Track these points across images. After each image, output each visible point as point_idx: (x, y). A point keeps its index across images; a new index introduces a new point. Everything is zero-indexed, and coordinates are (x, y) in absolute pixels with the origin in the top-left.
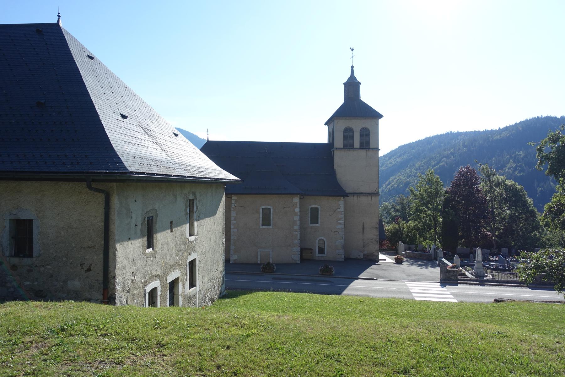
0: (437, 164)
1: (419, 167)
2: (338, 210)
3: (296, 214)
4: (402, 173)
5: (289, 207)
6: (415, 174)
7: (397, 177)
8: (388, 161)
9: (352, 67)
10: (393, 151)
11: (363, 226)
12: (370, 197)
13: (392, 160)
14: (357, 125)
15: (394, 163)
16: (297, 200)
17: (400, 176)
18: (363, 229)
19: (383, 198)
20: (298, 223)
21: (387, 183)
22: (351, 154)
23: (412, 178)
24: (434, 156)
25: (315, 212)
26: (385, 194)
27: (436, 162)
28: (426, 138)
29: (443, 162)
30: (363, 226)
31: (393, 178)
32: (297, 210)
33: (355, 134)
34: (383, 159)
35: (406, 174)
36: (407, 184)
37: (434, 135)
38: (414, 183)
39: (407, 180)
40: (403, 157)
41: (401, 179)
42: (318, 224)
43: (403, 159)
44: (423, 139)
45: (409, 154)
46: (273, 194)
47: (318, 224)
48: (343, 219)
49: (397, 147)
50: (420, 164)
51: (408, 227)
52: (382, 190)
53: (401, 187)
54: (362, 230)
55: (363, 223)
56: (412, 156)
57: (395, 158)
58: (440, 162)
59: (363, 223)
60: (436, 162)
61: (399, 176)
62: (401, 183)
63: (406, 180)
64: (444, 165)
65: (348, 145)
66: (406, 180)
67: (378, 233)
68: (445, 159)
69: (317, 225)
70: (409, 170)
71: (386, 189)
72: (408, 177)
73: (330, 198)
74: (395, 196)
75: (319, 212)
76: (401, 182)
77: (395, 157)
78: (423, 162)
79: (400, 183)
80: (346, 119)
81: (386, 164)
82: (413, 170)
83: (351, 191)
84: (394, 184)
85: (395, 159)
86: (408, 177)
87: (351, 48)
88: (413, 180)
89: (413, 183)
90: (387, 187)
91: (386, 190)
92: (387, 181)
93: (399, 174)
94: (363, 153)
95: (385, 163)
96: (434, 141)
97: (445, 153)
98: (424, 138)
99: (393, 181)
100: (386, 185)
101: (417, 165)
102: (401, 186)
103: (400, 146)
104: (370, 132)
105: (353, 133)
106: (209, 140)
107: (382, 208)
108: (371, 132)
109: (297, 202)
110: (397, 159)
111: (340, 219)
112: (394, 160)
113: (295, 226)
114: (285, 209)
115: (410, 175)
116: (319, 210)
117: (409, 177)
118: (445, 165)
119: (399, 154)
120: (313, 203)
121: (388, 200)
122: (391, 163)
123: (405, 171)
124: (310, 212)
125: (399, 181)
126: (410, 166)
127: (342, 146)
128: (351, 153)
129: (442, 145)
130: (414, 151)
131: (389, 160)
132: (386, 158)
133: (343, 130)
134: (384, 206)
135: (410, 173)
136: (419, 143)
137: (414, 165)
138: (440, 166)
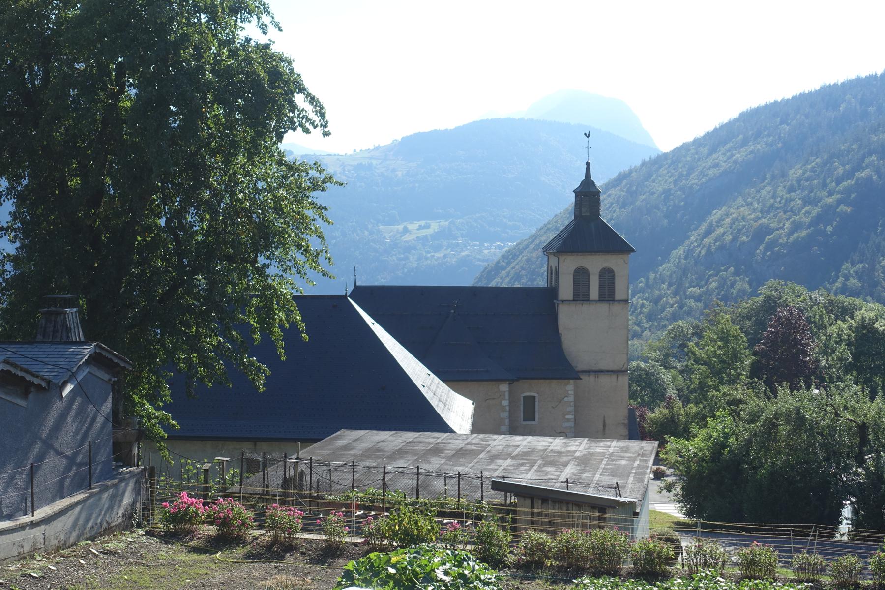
0: (849, 175)
1: (799, 181)
2: (566, 399)
3: (503, 409)
4: (749, 200)
5: (494, 399)
6: (785, 205)
7: (732, 210)
8: (707, 157)
9: (588, 164)
10: (723, 127)
11: (604, 421)
12: (614, 377)
13: (719, 157)
14: (595, 264)
15: (724, 166)
16: (504, 388)
17: (742, 209)
18: (604, 426)
19: (690, 275)
20: (507, 422)
21: (703, 227)
22: (585, 309)
23: (775, 216)
24: (843, 148)
25: (530, 402)
26: (696, 263)
27: (847, 167)
28: (824, 89)
29: (867, 167)
30: (604, 421)
31: (720, 212)
32: (505, 403)
33: (591, 277)
34: (693, 151)
35: (758, 204)
36: (761, 233)
37: (849, 78)
38: (781, 231)
39: (763, 220)
40: (752, 147)
41: (744, 218)
42: (534, 420)
43: (751, 152)
44: (816, 91)
45: (772, 138)
46: (471, 381)
47: (534, 420)
48: (573, 413)
49: (736, 115)
50: (801, 171)
51: (687, 414)
52: (689, 250)
53: (743, 243)
54: (602, 427)
55: (604, 417)
56: (780, 145)
57: (729, 151)
58: (859, 167)
59: (604, 417)
60: (847, 167)
61: (738, 208)
62: (744, 230)
63: (760, 222)
64: (869, 178)
65: (581, 296)
66: (760, 222)
67: (627, 433)
68: (874, 158)
69: (533, 423)
70: (768, 188)
71: (698, 246)
72: (765, 212)
73: (554, 381)
74: (726, 270)
75: (537, 403)
76: (744, 226)
77: (728, 145)
78: (809, 166)
79: (740, 230)
80: (577, 255)
81: (700, 168)
82: (781, 191)
83: (585, 368)
84: (724, 233)
85: (728, 154)
86: (765, 212)
87: (585, 134)
88: (779, 222)
89: (777, 232)
90: (702, 240)
91: (700, 252)
92: (702, 219)
93: (740, 200)
94: (604, 307)
95: (699, 163)
96: (848, 97)
97: (876, 139)
98: (818, 88)
99: (719, 222)
100: (699, 235)
101: (795, 173)
102: (745, 238)
103: (745, 110)
104: (614, 275)
105: (588, 275)
106: (358, 284)
107: (669, 333)
108: (616, 275)
109: (505, 392)
110: (734, 152)
111: (569, 413)
112: (724, 154)
113: (502, 427)
114: (488, 401)
115: (772, 206)
116: (537, 400)
117: (768, 212)
118: (875, 178)
119: (741, 136)
120: (528, 389)
121: (703, 283)
122: (716, 165)
123: (758, 191)
124: (522, 402)
125: (736, 223)
126: (773, 177)
127: (571, 298)
128: (585, 308)
129: (871, 109)
130: (787, 128)
131: (709, 154)
132: (701, 149)
133: (572, 272)
134: (674, 328)
135: (772, 201)
136: (802, 101)
137: (784, 175)
138: (858, 179)
